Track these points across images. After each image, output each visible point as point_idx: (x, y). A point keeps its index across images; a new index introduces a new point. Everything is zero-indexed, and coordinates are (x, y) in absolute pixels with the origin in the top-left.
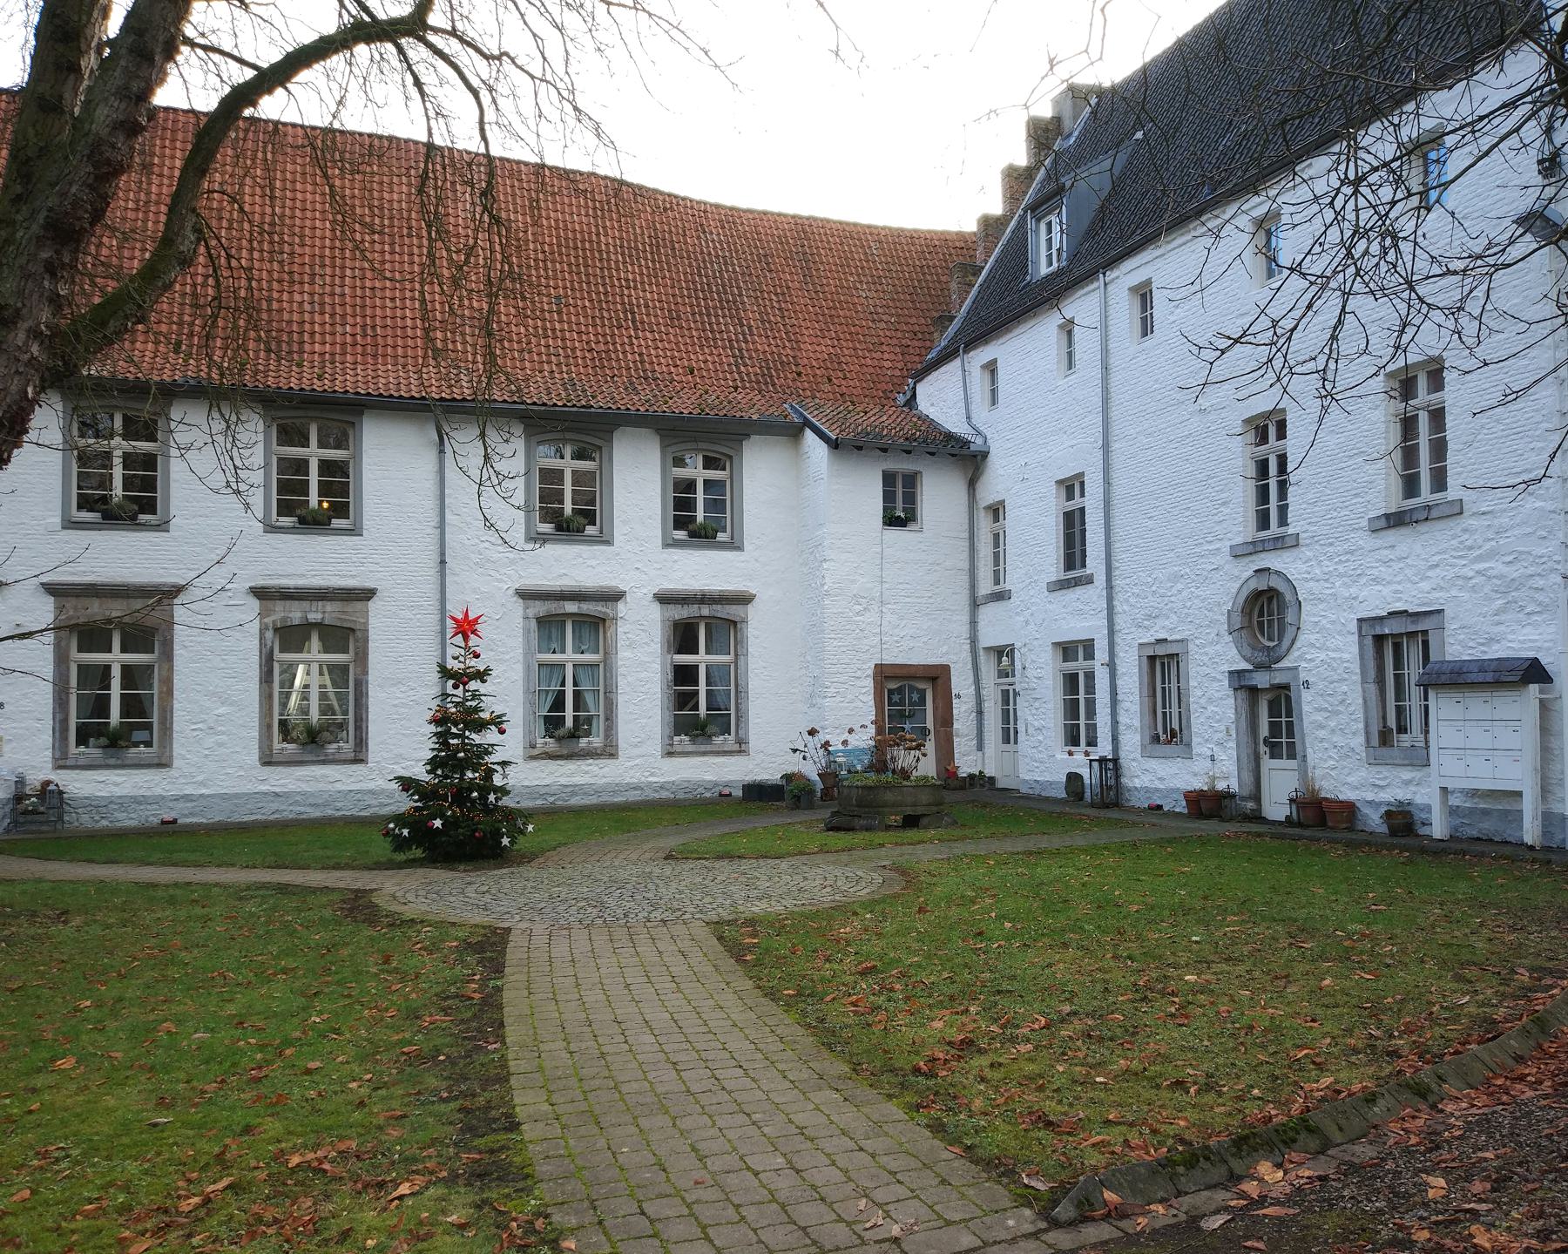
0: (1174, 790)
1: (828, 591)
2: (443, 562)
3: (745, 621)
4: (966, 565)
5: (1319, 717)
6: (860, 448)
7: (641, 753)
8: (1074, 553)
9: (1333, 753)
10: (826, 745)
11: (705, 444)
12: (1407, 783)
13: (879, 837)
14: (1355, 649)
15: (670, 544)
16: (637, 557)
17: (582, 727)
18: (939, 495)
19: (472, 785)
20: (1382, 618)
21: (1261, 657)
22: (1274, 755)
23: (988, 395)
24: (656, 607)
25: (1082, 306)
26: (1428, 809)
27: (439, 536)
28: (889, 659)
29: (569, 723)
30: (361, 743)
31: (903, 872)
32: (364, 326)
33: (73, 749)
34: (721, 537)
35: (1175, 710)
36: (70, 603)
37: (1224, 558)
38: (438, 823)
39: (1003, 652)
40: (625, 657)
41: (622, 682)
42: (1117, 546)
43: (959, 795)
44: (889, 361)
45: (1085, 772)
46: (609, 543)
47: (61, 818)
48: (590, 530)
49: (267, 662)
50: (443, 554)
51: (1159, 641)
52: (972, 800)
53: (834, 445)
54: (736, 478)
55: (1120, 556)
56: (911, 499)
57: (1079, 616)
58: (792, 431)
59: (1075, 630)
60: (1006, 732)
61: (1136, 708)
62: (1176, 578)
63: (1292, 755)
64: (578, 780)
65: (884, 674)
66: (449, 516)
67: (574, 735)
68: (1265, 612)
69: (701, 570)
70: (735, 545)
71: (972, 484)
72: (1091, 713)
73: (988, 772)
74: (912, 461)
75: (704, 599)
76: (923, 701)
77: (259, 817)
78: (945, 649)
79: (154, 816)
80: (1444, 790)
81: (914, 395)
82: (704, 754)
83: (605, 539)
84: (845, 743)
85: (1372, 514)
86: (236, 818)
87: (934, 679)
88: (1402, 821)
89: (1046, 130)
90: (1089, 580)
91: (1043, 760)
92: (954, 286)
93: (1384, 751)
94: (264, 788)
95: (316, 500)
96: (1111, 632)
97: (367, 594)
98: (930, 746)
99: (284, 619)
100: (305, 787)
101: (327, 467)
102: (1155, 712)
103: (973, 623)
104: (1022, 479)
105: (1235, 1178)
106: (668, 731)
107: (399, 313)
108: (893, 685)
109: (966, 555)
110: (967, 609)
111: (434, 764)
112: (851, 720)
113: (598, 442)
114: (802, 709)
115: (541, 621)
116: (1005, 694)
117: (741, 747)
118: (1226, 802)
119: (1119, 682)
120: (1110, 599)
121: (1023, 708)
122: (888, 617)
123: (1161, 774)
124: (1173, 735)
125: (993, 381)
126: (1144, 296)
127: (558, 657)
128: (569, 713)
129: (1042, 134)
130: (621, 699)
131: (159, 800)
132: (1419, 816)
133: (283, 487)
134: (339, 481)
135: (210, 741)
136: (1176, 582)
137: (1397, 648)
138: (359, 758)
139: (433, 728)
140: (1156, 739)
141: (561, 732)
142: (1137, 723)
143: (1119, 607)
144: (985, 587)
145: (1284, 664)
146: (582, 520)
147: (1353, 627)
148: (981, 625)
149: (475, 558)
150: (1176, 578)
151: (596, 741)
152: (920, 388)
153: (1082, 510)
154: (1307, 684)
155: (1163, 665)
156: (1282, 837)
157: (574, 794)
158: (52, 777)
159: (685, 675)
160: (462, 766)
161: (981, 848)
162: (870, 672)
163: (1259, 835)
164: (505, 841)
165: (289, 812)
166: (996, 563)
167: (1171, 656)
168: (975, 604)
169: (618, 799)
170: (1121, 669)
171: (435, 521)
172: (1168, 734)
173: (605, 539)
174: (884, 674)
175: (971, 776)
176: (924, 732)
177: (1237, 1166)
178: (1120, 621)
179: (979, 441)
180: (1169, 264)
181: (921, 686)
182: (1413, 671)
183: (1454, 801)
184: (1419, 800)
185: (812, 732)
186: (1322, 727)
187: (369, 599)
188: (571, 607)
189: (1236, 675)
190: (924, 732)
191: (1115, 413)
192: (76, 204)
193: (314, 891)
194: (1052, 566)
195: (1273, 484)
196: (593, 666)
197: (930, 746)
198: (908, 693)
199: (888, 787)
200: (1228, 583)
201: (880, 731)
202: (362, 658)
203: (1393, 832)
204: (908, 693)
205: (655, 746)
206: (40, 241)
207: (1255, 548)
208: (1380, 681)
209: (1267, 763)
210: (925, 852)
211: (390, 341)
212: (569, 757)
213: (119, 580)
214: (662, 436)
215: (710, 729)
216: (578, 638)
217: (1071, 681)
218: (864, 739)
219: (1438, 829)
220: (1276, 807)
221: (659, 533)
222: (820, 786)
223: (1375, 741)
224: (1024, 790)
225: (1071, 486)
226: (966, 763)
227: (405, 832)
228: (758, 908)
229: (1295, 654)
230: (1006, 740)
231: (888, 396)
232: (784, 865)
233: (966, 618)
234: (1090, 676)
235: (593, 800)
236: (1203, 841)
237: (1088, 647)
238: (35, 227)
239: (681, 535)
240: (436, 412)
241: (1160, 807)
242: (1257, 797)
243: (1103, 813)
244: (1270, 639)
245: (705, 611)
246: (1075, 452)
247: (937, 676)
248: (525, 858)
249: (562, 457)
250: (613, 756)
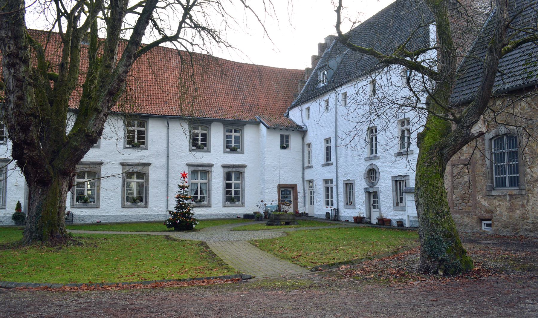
0: (351, 217)
1: (266, 165)
2: (168, 157)
3: (244, 172)
4: (301, 159)
5: (383, 199)
7: (217, 206)
10: (265, 204)
11: (234, 126)
12: (402, 215)
13: (280, 227)
15: (225, 152)
16: (217, 156)
17: (202, 199)
18: (295, 141)
19: (186, 213)
21: (371, 185)
22: (374, 208)
25: (331, 97)
26: (405, 221)
27: (168, 149)
28: (282, 183)
29: (199, 198)
30: (147, 203)
31: (286, 233)
32: (148, 96)
33: (75, 203)
34: (239, 150)
35: (352, 197)
37: (363, 161)
38: (178, 221)
39: (310, 181)
45: (330, 212)
46: (210, 152)
47: (72, 221)
48: (205, 148)
49: (124, 181)
50: (168, 154)
53: (268, 128)
54: (242, 135)
55: (339, 159)
56: (287, 142)
57: (329, 173)
58: (258, 124)
59: (328, 176)
61: (343, 196)
62: (352, 165)
63: (378, 208)
64: (201, 213)
65: (280, 187)
66: (170, 145)
67: (200, 201)
68: (372, 174)
70: (242, 152)
71: (303, 138)
73: (307, 212)
74: (289, 132)
75: (234, 166)
76: (290, 194)
77: (138, 220)
79: (95, 220)
80: (409, 216)
81: (288, 114)
83: (209, 151)
86: (115, 221)
87: (293, 188)
90: (332, 164)
91: (320, 209)
93: (397, 207)
94: (122, 214)
96: (337, 177)
97: (149, 165)
98: (292, 205)
100: (132, 214)
101: (203, 135)
102: (347, 197)
103: (303, 174)
104: (316, 137)
105: (338, 267)
108: (282, 189)
109: (301, 156)
110: (301, 170)
111: (177, 208)
112: (272, 199)
114: (259, 195)
116: (311, 192)
117: (243, 205)
120: (337, 169)
122: (281, 172)
127: (196, 181)
128: (199, 196)
129: (322, 47)
132: (404, 222)
133: (128, 137)
134: (142, 136)
135: (109, 202)
137: (400, 183)
138: (146, 207)
139: (176, 199)
140: (347, 204)
141: (197, 200)
142: (343, 200)
144: (306, 165)
146: (203, 146)
147: (391, 178)
148: (305, 174)
150: (352, 165)
151: (206, 203)
155: (349, 185)
157: (200, 216)
158: (70, 210)
159: (228, 186)
160: (182, 208)
161: (304, 229)
164: (194, 226)
165: (128, 220)
167: (351, 184)
168: (304, 169)
170: (339, 187)
172: (350, 203)
173: (209, 151)
174: (280, 187)
175: (302, 213)
176: (290, 201)
178: (339, 175)
179: (305, 127)
180: (349, 89)
181: (290, 189)
182: (404, 188)
183: (411, 219)
184: (404, 219)
185: (262, 201)
186: (384, 201)
188: (200, 168)
189: (366, 189)
191: (338, 123)
192: (114, 88)
194: (323, 160)
196: (206, 183)
197: (292, 205)
198: (286, 192)
199: (282, 215)
201: (279, 201)
202: (147, 181)
203: (398, 226)
204: (286, 192)
205: (221, 204)
206: (106, 95)
207: (369, 159)
209: (372, 210)
210: (291, 229)
212: (199, 207)
215: (235, 200)
216: (202, 177)
217: (327, 189)
218: (276, 203)
219: (407, 225)
220: (374, 221)
222: (264, 215)
223: (395, 205)
224: (315, 217)
225: (328, 141)
226: (301, 210)
228: (257, 239)
229: (378, 184)
230: (311, 204)
231: (282, 114)
232: (259, 232)
233: (301, 172)
234: (332, 188)
235: (205, 218)
237: (331, 181)
239: (228, 150)
240: (167, 118)
241: (348, 221)
242: (370, 218)
243: (334, 222)
246: (329, 133)
247: (294, 187)
250: (210, 207)
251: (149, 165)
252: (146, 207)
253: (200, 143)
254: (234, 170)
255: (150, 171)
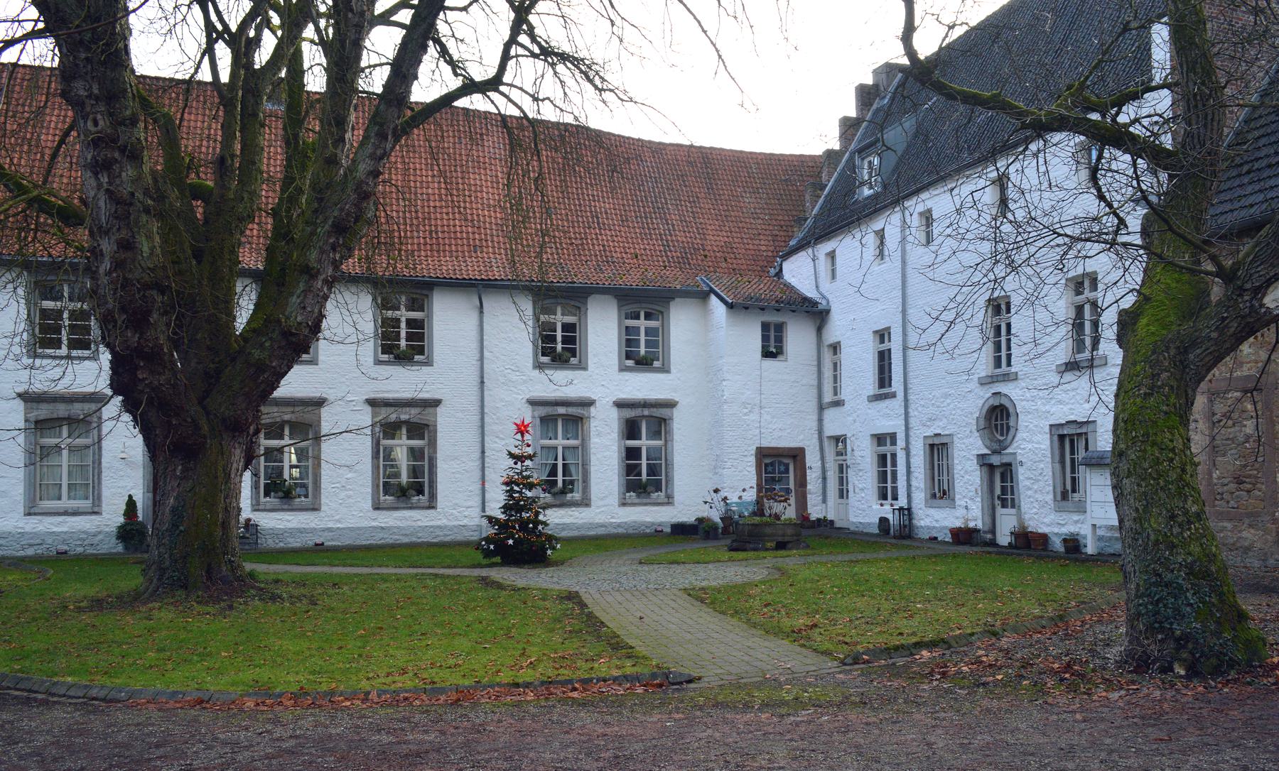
1: (725, 397)
4: (815, 383)
5: (1028, 483)
6: (747, 308)
7: (605, 504)
8: (884, 377)
9: (1035, 505)
10: (725, 499)
11: (645, 303)
12: (1076, 522)
14: (1048, 443)
15: (623, 369)
16: (602, 379)
17: (568, 486)
18: (798, 338)
19: (529, 521)
20: (1062, 425)
21: (996, 446)
23: (830, 273)
24: (615, 410)
25: (891, 223)
28: (765, 444)
29: (560, 484)
31: (779, 570)
32: (431, 232)
33: (262, 499)
34: (656, 364)
35: (945, 478)
37: (974, 385)
38: (511, 542)
39: (838, 439)
41: (593, 458)
42: (911, 374)
43: (811, 532)
44: (764, 245)
46: (585, 369)
50: (482, 377)
51: (936, 435)
52: (817, 534)
53: (731, 306)
55: (913, 381)
56: (780, 340)
57: (887, 418)
58: (703, 296)
59: (885, 426)
60: (841, 491)
62: (947, 396)
63: (1013, 506)
64: (567, 520)
66: (486, 354)
67: (563, 492)
68: (998, 418)
69: (643, 386)
70: (665, 369)
71: (819, 330)
72: (895, 479)
73: (830, 517)
74: (782, 316)
75: (645, 404)
76: (787, 471)
77: (414, 539)
78: (801, 437)
79: (310, 541)
80: (1094, 526)
81: (781, 270)
82: (646, 504)
83: (582, 366)
84: (740, 498)
85: (1059, 362)
86: (358, 542)
88: (1073, 545)
89: (869, 93)
90: (893, 395)
91: (865, 509)
92: (808, 197)
93: (1064, 503)
94: (374, 524)
95: (404, 344)
97: (436, 403)
98: (792, 501)
100: (399, 524)
103: (820, 420)
104: (852, 327)
105: (912, 654)
106: (623, 489)
107: (452, 223)
108: (768, 461)
111: (506, 508)
112: (741, 485)
113: (577, 304)
114: (713, 474)
116: (841, 467)
117: (669, 501)
118: (975, 535)
119: (912, 460)
120: (906, 407)
121: (852, 475)
122: (765, 417)
123: (937, 517)
124: (944, 493)
125: (833, 264)
126: (927, 219)
127: (553, 442)
128: (560, 478)
129: (866, 95)
130: (592, 469)
131: (313, 531)
132: (1082, 541)
133: (385, 336)
134: (418, 332)
135: (343, 495)
136: (946, 399)
137: (1072, 442)
139: (504, 488)
140: (934, 496)
142: (922, 486)
143: (912, 413)
144: (828, 397)
145: (1009, 450)
147: (1047, 429)
149: (502, 379)
150: (947, 396)
151: (577, 496)
152: (785, 265)
153: (889, 350)
154: (1021, 463)
156: (1008, 554)
157: (563, 529)
158: (251, 516)
159: (632, 453)
163: (990, 553)
166: (835, 381)
168: (821, 408)
169: (592, 533)
170: (913, 452)
171: (477, 356)
172: (941, 493)
173: (582, 366)
175: (819, 520)
176: (788, 491)
177: (914, 651)
178: (912, 421)
179: (824, 302)
180: (939, 201)
181: (786, 461)
182: (1081, 454)
183: (1100, 532)
184: (1082, 532)
186: (1030, 489)
188: (561, 410)
190: (788, 491)
191: (909, 291)
193: (448, 576)
194: (871, 386)
195: (1003, 339)
197: (792, 501)
198: (778, 466)
199: (767, 524)
200: (976, 401)
201: (759, 491)
202: (433, 443)
203: (1068, 550)
204: (778, 466)
205: (614, 499)
206: (329, 234)
208: (1062, 462)
210: (792, 560)
211: (447, 241)
212: (561, 506)
213: (289, 395)
214: (619, 301)
215: (650, 489)
216: (565, 431)
217: (882, 459)
218: (751, 496)
219: (1090, 549)
220: (1004, 539)
221: (616, 362)
222: (721, 525)
223: (1059, 498)
224: (852, 528)
225: (883, 335)
226: (815, 512)
227: (492, 547)
228: (704, 584)
229: (1015, 445)
230: (841, 496)
231: (763, 271)
232: (710, 566)
233: (815, 417)
234: (894, 456)
235: (576, 533)
236: (955, 556)
237: (893, 437)
238: (327, 227)
240: (478, 287)
241: (936, 538)
244: (1002, 435)
245: (646, 412)
246: (886, 314)
247: (797, 455)
248: (556, 564)
250: (588, 505)
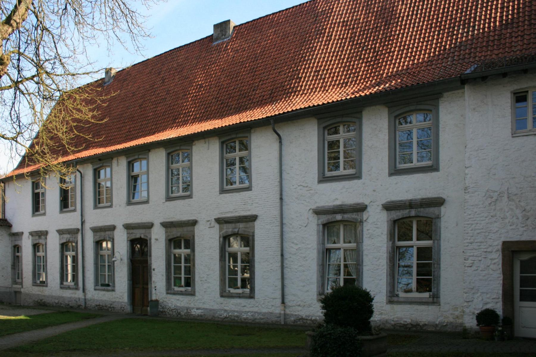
24: (385, 213)
36: (225, 226)
40: (367, 244)
50: (281, 194)
75: (411, 205)
97: (254, 218)
99: (226, 232)
101: (241, 160)
115: (324, 225)
130: (365, 269)
162: (500, 247)
187: (255, 220)
188: (339, 217)
249: (402, 125)
251: (194, 223)
252: (113, 290)
253: (336, 163)
254: (413, 213)
255: (256, 232)
